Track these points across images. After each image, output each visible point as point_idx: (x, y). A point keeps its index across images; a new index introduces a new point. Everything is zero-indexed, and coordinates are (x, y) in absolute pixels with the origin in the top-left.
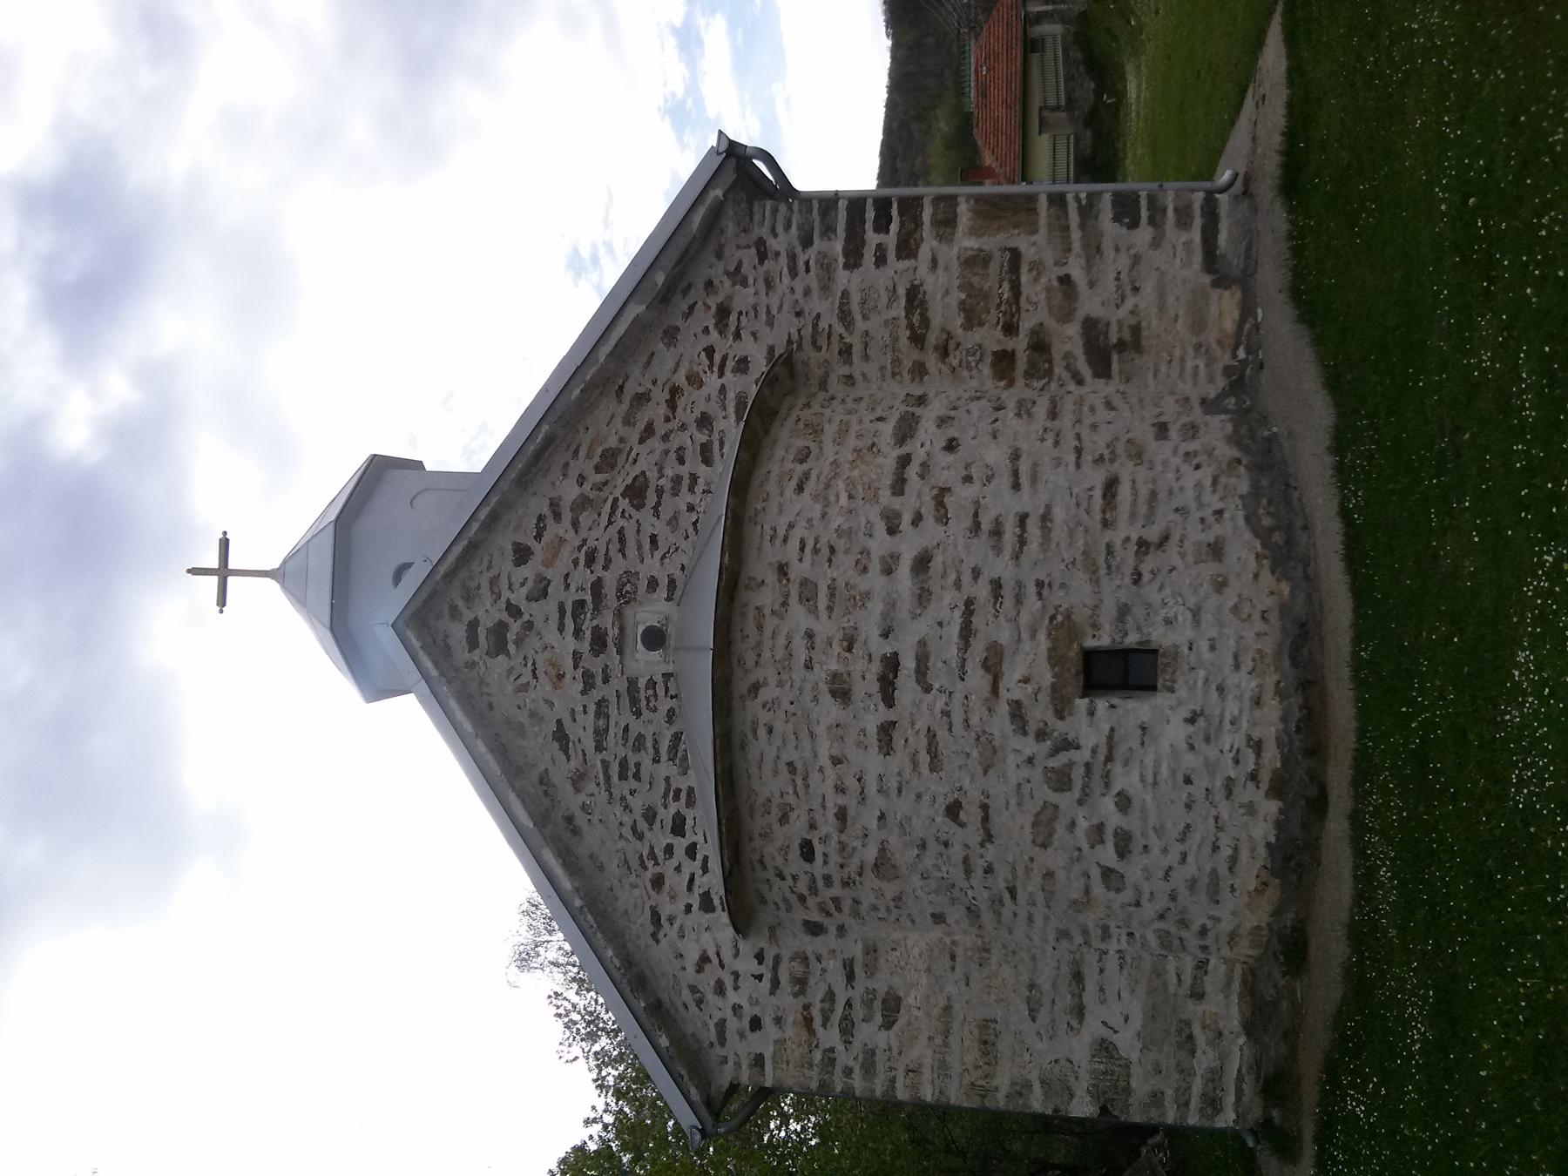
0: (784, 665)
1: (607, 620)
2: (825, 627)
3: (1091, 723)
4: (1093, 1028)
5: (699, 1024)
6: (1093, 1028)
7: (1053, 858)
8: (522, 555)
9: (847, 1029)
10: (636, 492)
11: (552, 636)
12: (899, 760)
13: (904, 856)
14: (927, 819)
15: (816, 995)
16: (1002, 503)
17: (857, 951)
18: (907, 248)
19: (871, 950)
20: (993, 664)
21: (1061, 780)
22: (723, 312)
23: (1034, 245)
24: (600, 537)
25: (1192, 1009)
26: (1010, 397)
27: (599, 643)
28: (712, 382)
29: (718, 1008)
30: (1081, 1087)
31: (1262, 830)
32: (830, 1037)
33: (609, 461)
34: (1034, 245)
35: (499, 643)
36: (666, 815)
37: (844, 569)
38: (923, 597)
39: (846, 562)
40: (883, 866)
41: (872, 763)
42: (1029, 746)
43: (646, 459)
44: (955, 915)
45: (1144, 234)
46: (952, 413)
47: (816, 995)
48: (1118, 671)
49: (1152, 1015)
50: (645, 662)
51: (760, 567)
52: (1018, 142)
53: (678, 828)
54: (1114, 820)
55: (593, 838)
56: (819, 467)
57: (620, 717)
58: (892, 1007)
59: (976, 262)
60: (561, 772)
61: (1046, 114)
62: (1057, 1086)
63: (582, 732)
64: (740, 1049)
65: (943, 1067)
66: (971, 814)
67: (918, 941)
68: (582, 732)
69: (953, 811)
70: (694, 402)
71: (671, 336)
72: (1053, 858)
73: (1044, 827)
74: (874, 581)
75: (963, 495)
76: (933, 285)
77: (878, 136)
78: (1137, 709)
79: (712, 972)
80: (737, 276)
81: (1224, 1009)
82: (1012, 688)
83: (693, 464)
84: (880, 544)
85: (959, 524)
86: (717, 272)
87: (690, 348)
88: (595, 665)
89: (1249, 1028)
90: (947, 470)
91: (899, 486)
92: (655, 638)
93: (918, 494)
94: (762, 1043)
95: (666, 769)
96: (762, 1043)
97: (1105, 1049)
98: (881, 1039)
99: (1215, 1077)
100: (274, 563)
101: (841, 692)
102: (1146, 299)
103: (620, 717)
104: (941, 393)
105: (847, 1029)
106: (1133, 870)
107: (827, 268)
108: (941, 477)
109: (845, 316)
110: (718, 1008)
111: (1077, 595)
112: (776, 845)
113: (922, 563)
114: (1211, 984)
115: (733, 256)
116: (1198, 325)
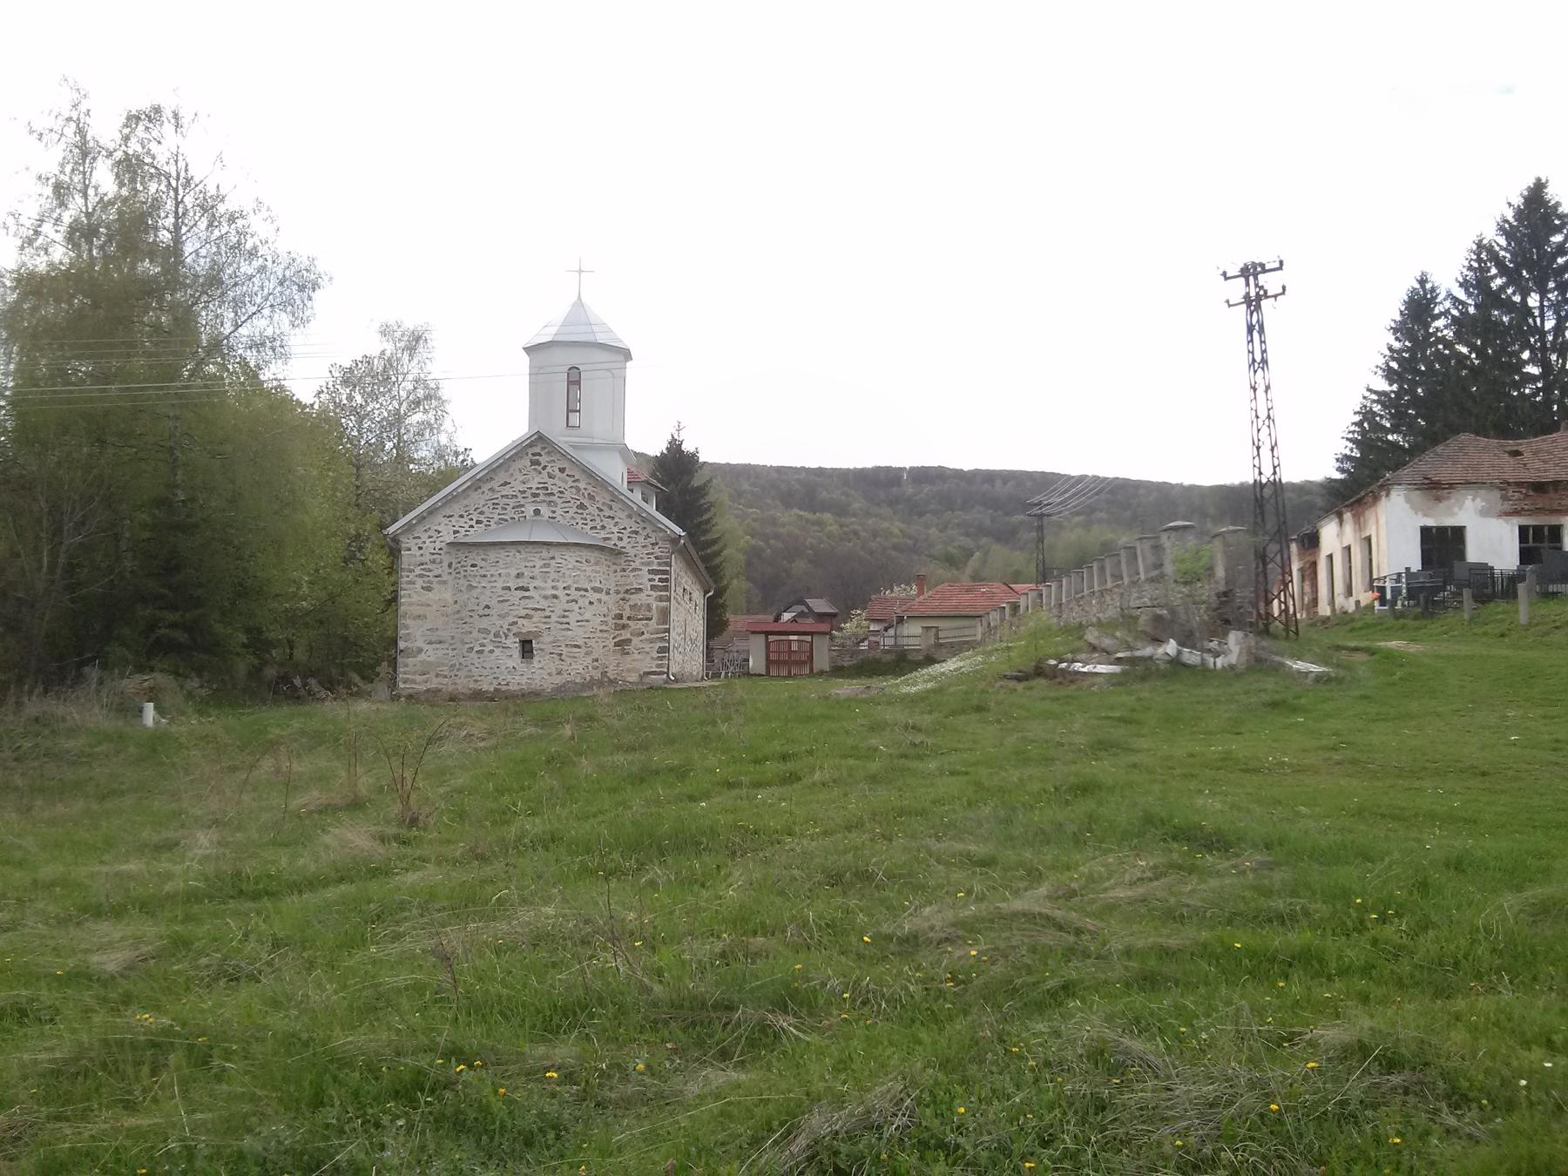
0: (526, 560)
1: (542, 498)
2: (537, 571)
3: (513, 644)
4: (426, 647)
5: (419, 531)
6: (426, 647)
7: (475, 634)
8: (562, 470)
9: (421, 576)
10: (582, 506)
11: (538, 479)
13: (475, 593)
14: (484, 601)
16: (573, 618)
17: (444, 578)
18: (653, 588)
19: (445, 582)
20: (527, 617)
22: (636, 533)
23: (653, 624)
24: (568, 495)
25: (432, 674)
26: (609, 619)
27: (535, 495)
28: (615, 530)
29: (424, 537)
30: (409, 644)
31: (485, 687)
32: (418, 571)
33: (591, 497)
34: (653, 624)
35: (534, 463)
36: (482, 518)
37: (553, 575)
38: (546, 597)
39: (555, 576)
40: (471, 587)
41: (500, 585)
42: (506, 626)
43: (592, 509)
44: (457, 607)
45: (656, 655)
48: (527, 648)
49: (430, 663)
51: (553, 552)
53: (478, 522)
54: (487, 649)
55: (474, 495)
56: (585, 566)
58: (429, 589)
60: (494, 484)
62: (408, 637)
63: (507, 491)
64: (412, 543)
65: (411, 604)
66: (487, 611)
67: (448, 596)
68: (507, 491)
69: (487, 607)
70: (609, 524)
71: (630, 516)
72: (475, 634)
73: (486, 631)
74: (550, 584)
75: (575, 607)
76: (643, 595)
78: (516, 653)
80: (648, 536)
81: (434, 683)
82: (521, 621)
83: (591, 524)
84: (561, 585)
85: (567, 607)
86: (649, 530)
87: (626, 523)
89: (428, 690)
90: (583, 602)
91: (577, 589)
92: (537, 512)
93: (575, 594)
95: (497, 517)
96: (415, 550)
97: (420, 650)
98: (418, 586)
99: (414, 682)
100: (584, 300)
101: (518, 576)
102: (636, 656)
103: (512, 502)
104: (611, 600)
105: (421, 576)
107: (648, 564)
108: (581, 602)
109: (634, 570)
110: (424, 537)
111: (547, 639)
112: (475, 557)
113: (555, 597)
114: (440, 679)
115: (653, 535)
116: (629, 670)
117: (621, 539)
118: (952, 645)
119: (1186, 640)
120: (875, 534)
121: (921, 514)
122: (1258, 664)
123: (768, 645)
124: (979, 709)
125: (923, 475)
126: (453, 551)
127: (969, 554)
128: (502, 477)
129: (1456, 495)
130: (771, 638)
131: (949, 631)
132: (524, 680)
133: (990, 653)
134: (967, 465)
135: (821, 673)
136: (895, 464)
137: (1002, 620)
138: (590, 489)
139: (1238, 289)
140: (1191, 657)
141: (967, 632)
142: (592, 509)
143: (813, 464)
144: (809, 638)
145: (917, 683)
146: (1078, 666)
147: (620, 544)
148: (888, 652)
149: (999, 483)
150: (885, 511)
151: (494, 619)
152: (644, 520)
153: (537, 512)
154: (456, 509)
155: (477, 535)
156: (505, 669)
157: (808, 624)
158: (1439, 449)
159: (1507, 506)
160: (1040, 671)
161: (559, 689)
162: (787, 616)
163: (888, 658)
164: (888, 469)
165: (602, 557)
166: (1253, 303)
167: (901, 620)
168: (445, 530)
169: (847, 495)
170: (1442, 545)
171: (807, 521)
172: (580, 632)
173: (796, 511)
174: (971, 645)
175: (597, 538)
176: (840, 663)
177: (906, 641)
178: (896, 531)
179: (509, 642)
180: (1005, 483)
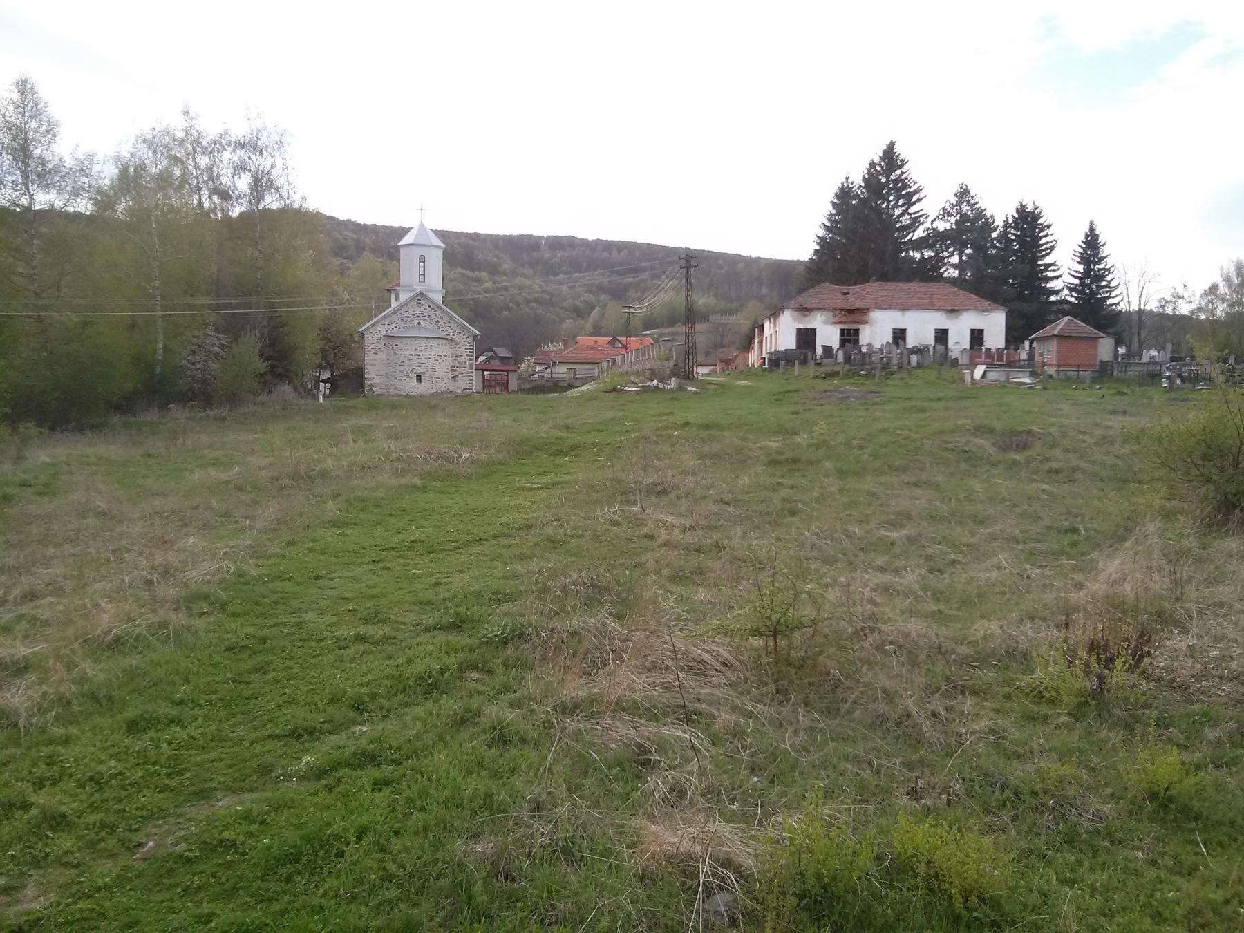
14: (402, 359)
46: (104, 703)
48: (419, 378)
67: (384, 356)
77: (716, 250)
112: (397, 342)
119: (662, 380)
122: (680, 388)
125: (557, 243)
129: (813, 314)
135: (513, 392)
136: (536, 233)
139: (683, 263)
140: (661, 385)
143: (470, 230)
145: (574, 393)
149: (615, 252)
150: (527, 270)
154: (387, 321)
157: (496, 363)
158: (811, 290)
159: (836, 319)
160: (615, 390)
161: (432, 395)
162: (482, 358)
163: (549, 384)
164: (530, 237)
166: (688, 268)
167: (554, 364)
168: (382, 330)
170: (806, 338)
173: (459, 270)
174: (593, 379)
178: (537, 289)
180: (619, 252)
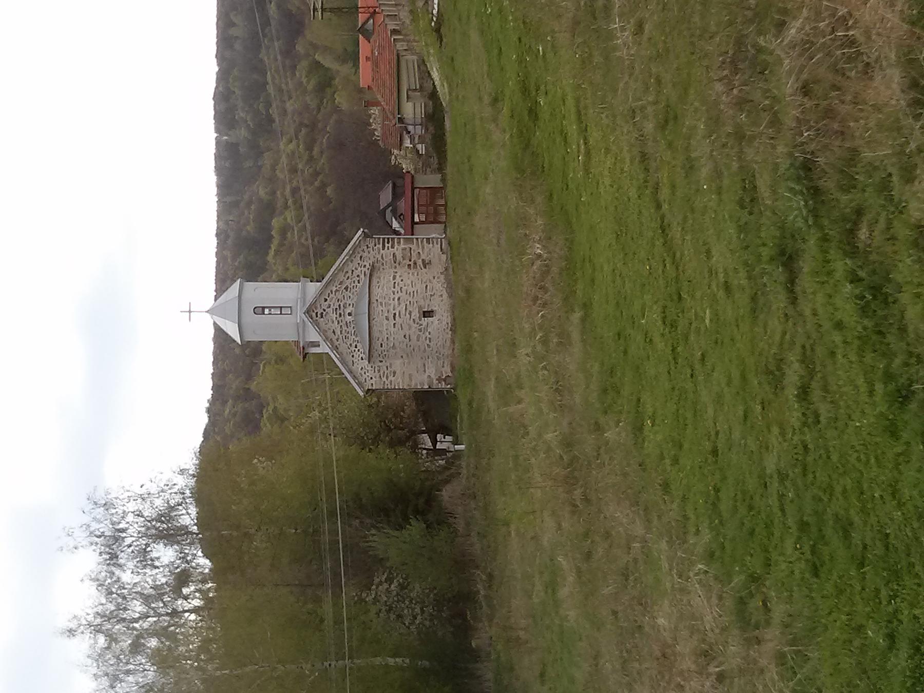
2: (384, 309)
8: (326, 300)
9: (387, 378)
10: (346, 288)
12: (396, 329)
13: (397, 344)
15: (382, 372)
16: (411, 290)
18: (393, 247)
21: (420, 330)
23: (414, 247)
24: (340, 297)
26: (411, 272)
32: (384, 379)
33: (341, 283)
34: (414, 247)
38: (399, 304)
43: (348, 283)
47: (382, 372)
48: (428, 314)
50: (349, 318)
51: (373, 300)
52: (396, 94)
56: (381, 284)
57: (344, 328)
58: (395, 373)
59: (404, 249)
61: (410, 93)
63: (338, 332)
66: (407, 337)
68: (338, 332)
70: (356, 273)
75: (404, 288)
79: (364, 370)
82: (413, 317)
84: (392, 296)
88: (340, 319)
92: (350, 314)
94: (373, 382)
96: (373, 382)
101: (387, 319)
103: (344, 328)
105: (387, 378)
106: (431, 344)
111: (422, 303)
113: (399, 299)
116: (440, 260)
117: (365, 266)
118: (421, 78)
120: (294, 170)
121: (271, 121)
123: (421, 222)
124: (452, 59)
125: (225, 118)
126: (372, 360)
127: (317, 66)
128: (330, 334)
130: (416, 219)
131: (410, 79)
132: (445, 315)
133: (428, 53)
134: (211, 68)
137: (403, 40)
138: (337, 284)
141: (411, 65)
142: (348, 283)
143: (212, 244)
144: (416, 191)
146: (435, 12)
147: (368, 266)
148: (427, 130)
149: (233, 32)
150: (267, 160)
151: (411, 332)
152: (354, 253)
153: (350, 314)
154: (349, 359)
155: (363, 347)
156: (440, 323)
157: (403, 205)
160: (438, 30)
161: (450, 296)
162: (395, 225)
163: (431, 128)
164: (218, 157)
165: (375, 275)
167: (401, 120)
169: (249, 203)
171: (281, 244)
172: (418, 286)
174: (422, 63)
175: (364, 280)
176: (435, 166)
177: (418, 116)
178: (291, 147)
179: (425, 324)
180: (233, 25)
